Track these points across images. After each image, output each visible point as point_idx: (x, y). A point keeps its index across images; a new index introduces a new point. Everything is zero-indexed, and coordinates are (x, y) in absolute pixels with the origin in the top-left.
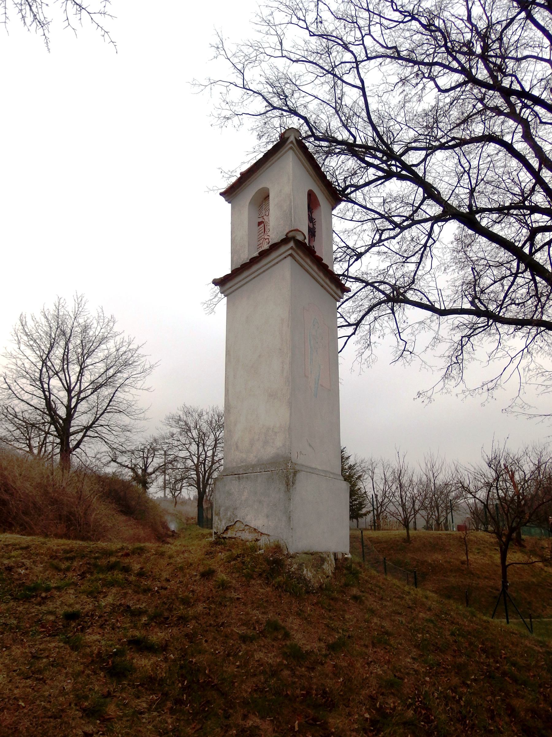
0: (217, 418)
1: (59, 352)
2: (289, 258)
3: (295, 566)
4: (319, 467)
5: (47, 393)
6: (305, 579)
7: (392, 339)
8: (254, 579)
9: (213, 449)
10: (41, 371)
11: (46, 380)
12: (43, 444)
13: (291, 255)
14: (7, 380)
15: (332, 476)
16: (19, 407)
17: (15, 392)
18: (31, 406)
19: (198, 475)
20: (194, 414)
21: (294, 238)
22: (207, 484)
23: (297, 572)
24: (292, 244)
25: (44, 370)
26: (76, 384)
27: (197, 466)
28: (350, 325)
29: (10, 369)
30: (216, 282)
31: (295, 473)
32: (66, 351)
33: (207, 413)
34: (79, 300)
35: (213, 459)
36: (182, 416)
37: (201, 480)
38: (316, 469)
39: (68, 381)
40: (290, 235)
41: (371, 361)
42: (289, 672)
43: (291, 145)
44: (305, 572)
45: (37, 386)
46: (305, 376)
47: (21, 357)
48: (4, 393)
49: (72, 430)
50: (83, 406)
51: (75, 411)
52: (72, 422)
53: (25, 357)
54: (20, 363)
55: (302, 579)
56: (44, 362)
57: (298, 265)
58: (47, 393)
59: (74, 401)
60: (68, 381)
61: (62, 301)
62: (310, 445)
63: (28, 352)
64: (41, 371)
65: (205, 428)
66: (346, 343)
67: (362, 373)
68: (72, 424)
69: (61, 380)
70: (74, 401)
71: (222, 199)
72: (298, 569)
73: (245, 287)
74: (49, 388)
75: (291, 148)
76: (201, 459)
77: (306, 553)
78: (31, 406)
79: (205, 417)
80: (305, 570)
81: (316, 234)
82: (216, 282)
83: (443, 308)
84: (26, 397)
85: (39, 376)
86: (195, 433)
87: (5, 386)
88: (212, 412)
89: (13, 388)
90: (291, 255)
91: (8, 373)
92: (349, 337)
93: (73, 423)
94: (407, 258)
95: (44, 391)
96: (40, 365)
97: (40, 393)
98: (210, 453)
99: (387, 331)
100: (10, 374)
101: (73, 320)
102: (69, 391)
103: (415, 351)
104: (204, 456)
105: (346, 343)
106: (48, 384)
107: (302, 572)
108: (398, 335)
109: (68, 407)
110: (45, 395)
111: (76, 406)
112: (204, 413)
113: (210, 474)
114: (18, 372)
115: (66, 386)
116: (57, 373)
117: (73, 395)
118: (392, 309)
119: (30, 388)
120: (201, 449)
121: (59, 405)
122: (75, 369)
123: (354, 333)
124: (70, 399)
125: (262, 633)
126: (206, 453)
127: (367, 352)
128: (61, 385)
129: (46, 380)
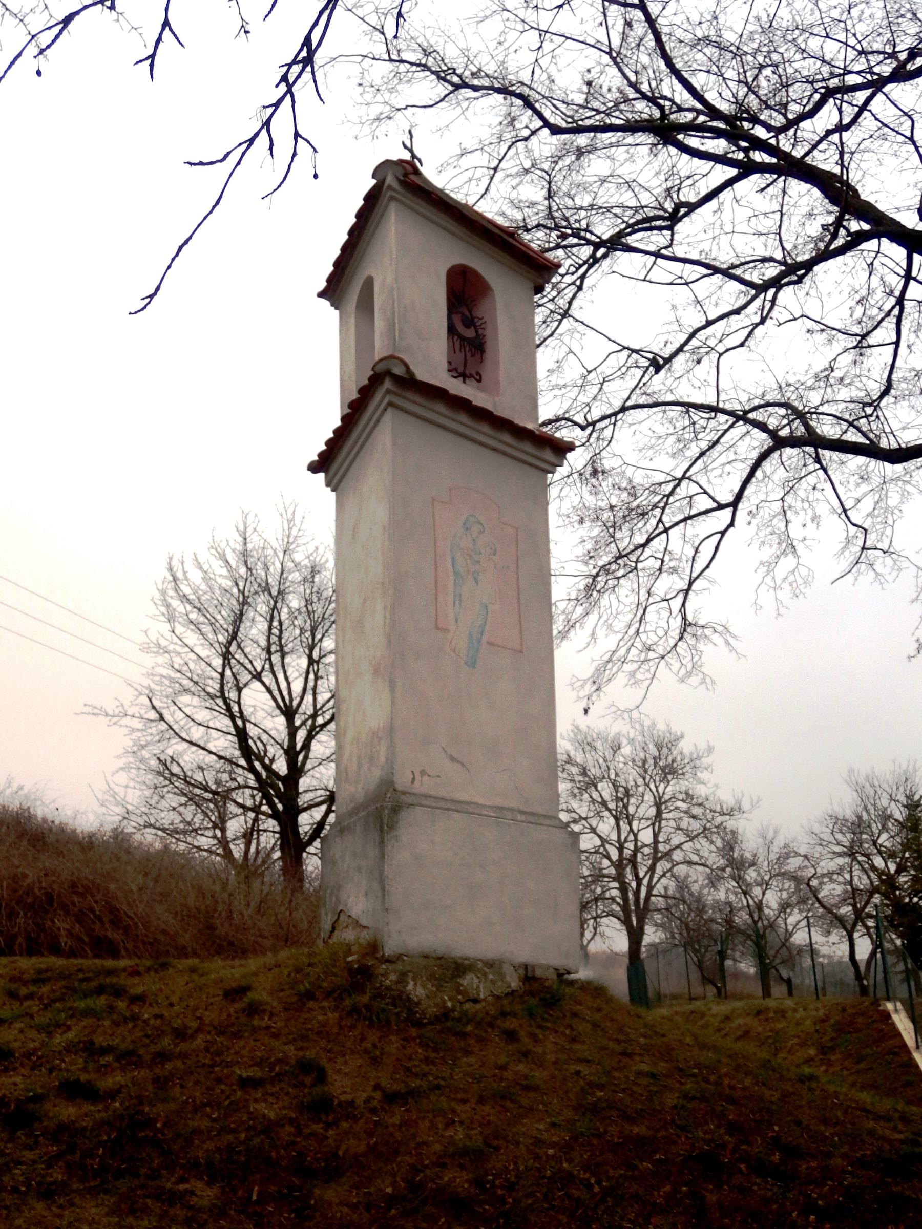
0: (653, 750)
1: (255, 630)
2: (390, 411)
3: (393, 977)
4: (480, 801)
5: (239, 722)
6: (409, 999)
7: (835, 527)
8: (316, 1000)
9: (653, 824)
10: (222, 675)
11: (233, 695)
12: (248, 836)
13: (390, 404)
14: (156, 703)
15: (523, 818)
16: (190, 758)
17: (175, 727)
18: (211, 752)
19: (623, 889)
20: (598, 744)
21: (388, 373)
22: (646, 908)
23: (394, 987)
24: (388, 384)
25: (228, 673)
26: (302, 698)
27: (619, 865)
28: (721, 507)
29: (157, 678)
30: (314, 468)
31: (396, 809)
32: (275, 624)
33: (631, 741)
34: (290, 512)
35: (656, 850)
36: (572, 753)
37: (631, 902)
38: (469, 803)
39: (285, 693)
40: (381, 368)
41: (800, 581)
42: (292, 1129)
43: (390, 193)
44: (410, 987)
45: (217, 708)
46: (437, 628)
47: (179, 649)
48: (150, 731)
49: (303, 800)
50: (323, 745)
51: (306, 758)
52: (301, 781)
53: (187, 649)
54: (178, 661)
55: (402, 1000)
56: (226, 657)
57: (413, 419)
58: (239, 722)
59: (301, 735)
60: (285, 693)
61: (250, 519)
62: (452, 759)
63: (192, 638)
64: (222, 675)
65: (631, 776)
66: (717, 548)
67: (782, 611)
68: (301, 790)
69: (269, 690)
70: (301, 735)
71: (325, 303)
72: (397, 982)
73: (352, 470)
74: (241, 712)
75: (392, 198)
76: (626, 851)
77: (426, 957)
78: (211, 752)
79: (626, 750)
80: (412, 983)
81: (489, 347)
82: (314, 468)
83: (894, 445)
84: (197, 734)
85: (217, 686)
86: (606, 790)
87: (153, 715)
88: (640, 738)
89: (167, 717)
90: (390, 404)
91: (153, 686)
92: (723, 533)
93: (304, 783)
94: (864, 337)
95: (232, 717)
96: (218, 662)
97: (225, 723)
98: (646, 837)
99: (822, 509)
100: (158, 688)
101: (281, 555)
102: (289, 713)
103: (897, 546)
104: (631, 846)
105: (717, 548)
106: (239, 703)
107: (404, 987)
108: (843, 516)
109: (291, 753)
110: (236, 726)
111: (306, 746)
112: (624, 742)
113: (650, 887)
114: (172, 680)
115: (282, 704)
116: (258, 676)
117: (297, 723)
118: (818, 460)
119: (203, 715)
120: (624, 826)
121: (272, 750)
122: (297, 663)
123: (732, 524)
124: (292, 731)
125: (279, 1077)
126: (635, 835)
127: (788, 562)
128: (272, 703)
129: (233, 695)
